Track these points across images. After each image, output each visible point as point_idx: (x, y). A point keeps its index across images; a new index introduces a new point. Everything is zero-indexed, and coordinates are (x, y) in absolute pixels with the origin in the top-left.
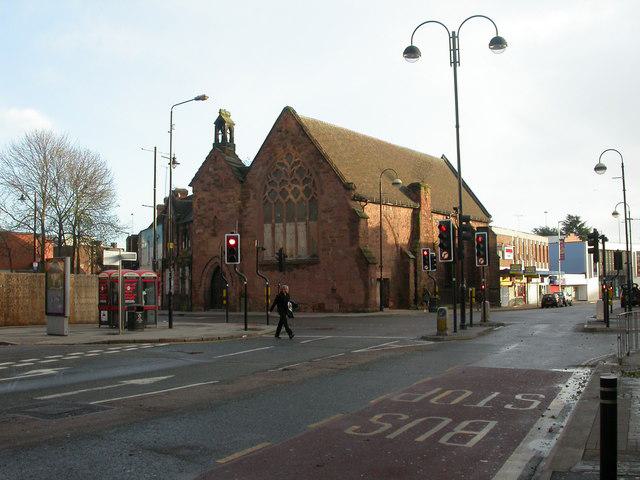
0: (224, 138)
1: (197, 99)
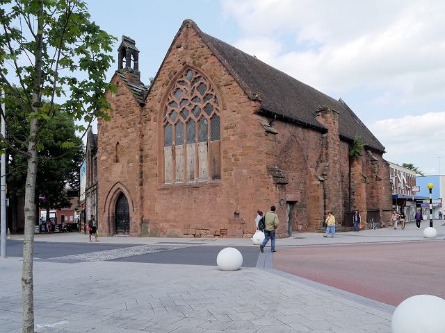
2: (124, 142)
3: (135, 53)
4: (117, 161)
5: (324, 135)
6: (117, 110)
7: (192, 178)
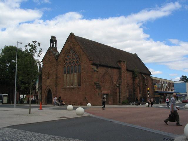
0: (53, 45)
1: (22, 43)
2: (51, 72)
3: (56, 41)
4: (48, 78)
5: (120, 70)
7: (72, 85)
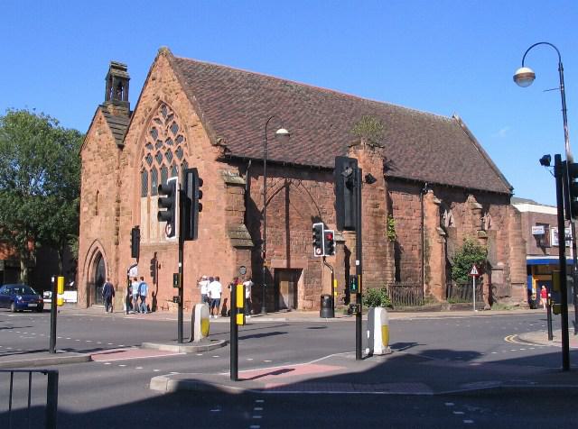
4: (97, 214)
6: (98, 151)
